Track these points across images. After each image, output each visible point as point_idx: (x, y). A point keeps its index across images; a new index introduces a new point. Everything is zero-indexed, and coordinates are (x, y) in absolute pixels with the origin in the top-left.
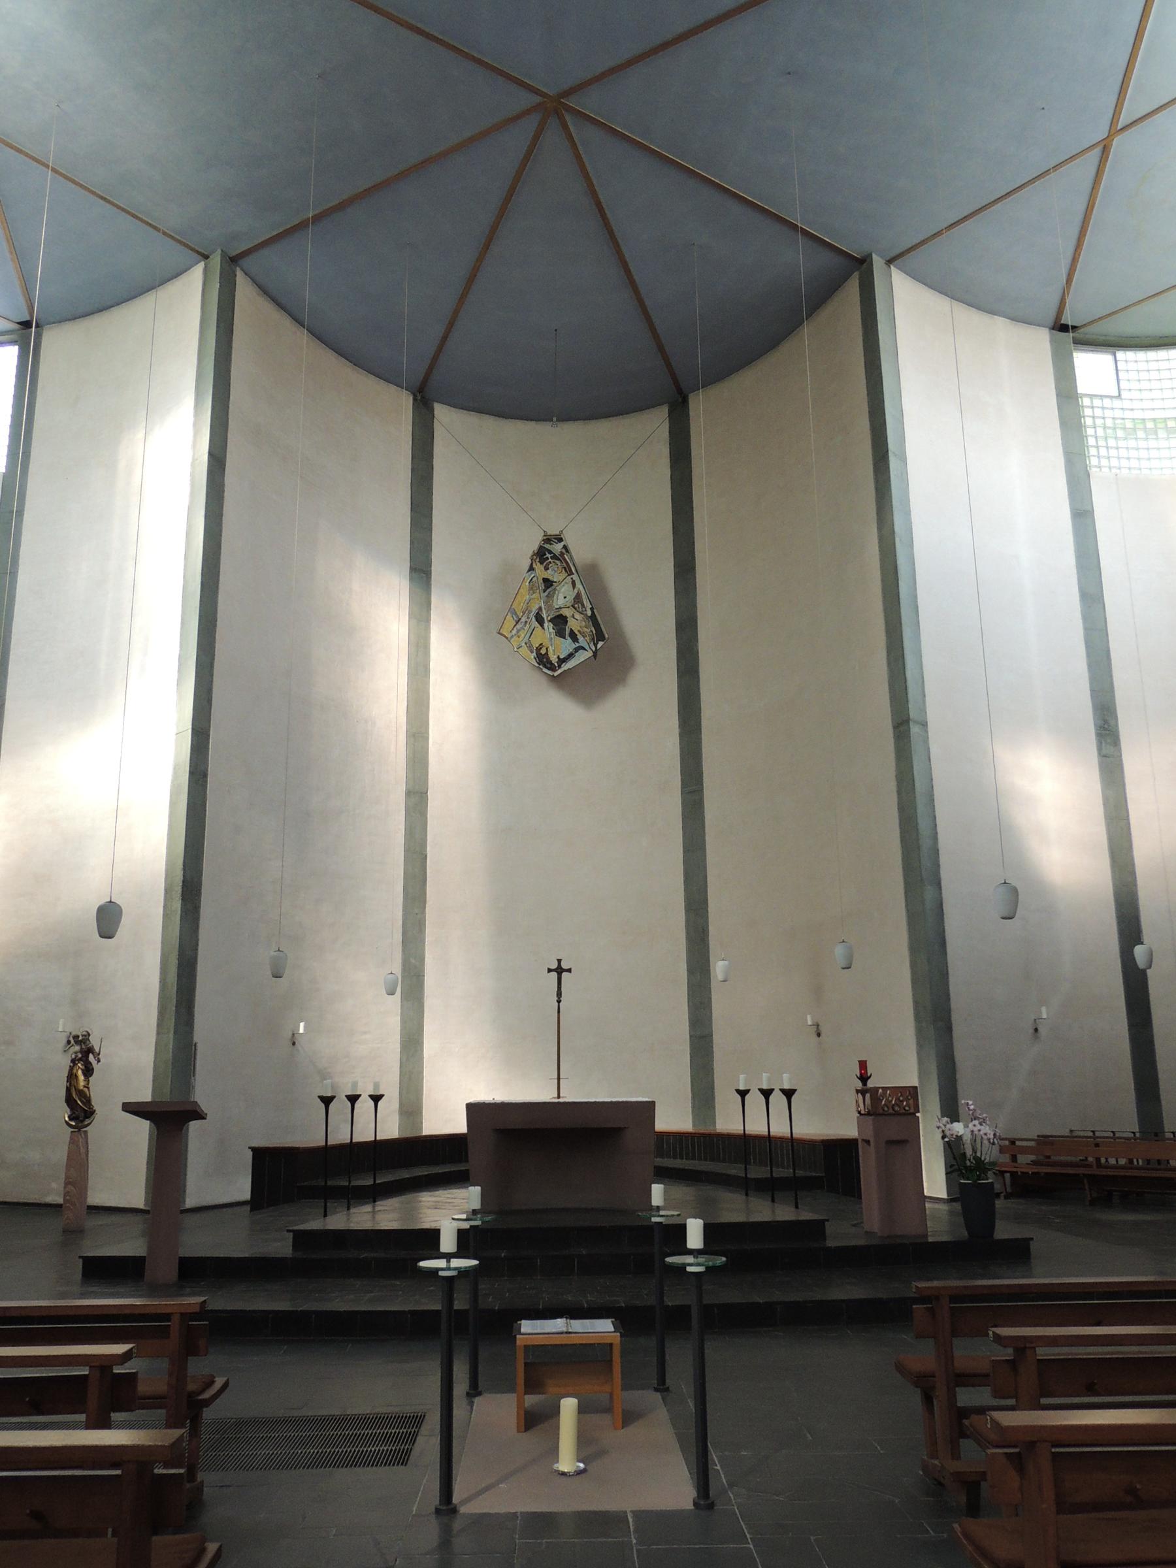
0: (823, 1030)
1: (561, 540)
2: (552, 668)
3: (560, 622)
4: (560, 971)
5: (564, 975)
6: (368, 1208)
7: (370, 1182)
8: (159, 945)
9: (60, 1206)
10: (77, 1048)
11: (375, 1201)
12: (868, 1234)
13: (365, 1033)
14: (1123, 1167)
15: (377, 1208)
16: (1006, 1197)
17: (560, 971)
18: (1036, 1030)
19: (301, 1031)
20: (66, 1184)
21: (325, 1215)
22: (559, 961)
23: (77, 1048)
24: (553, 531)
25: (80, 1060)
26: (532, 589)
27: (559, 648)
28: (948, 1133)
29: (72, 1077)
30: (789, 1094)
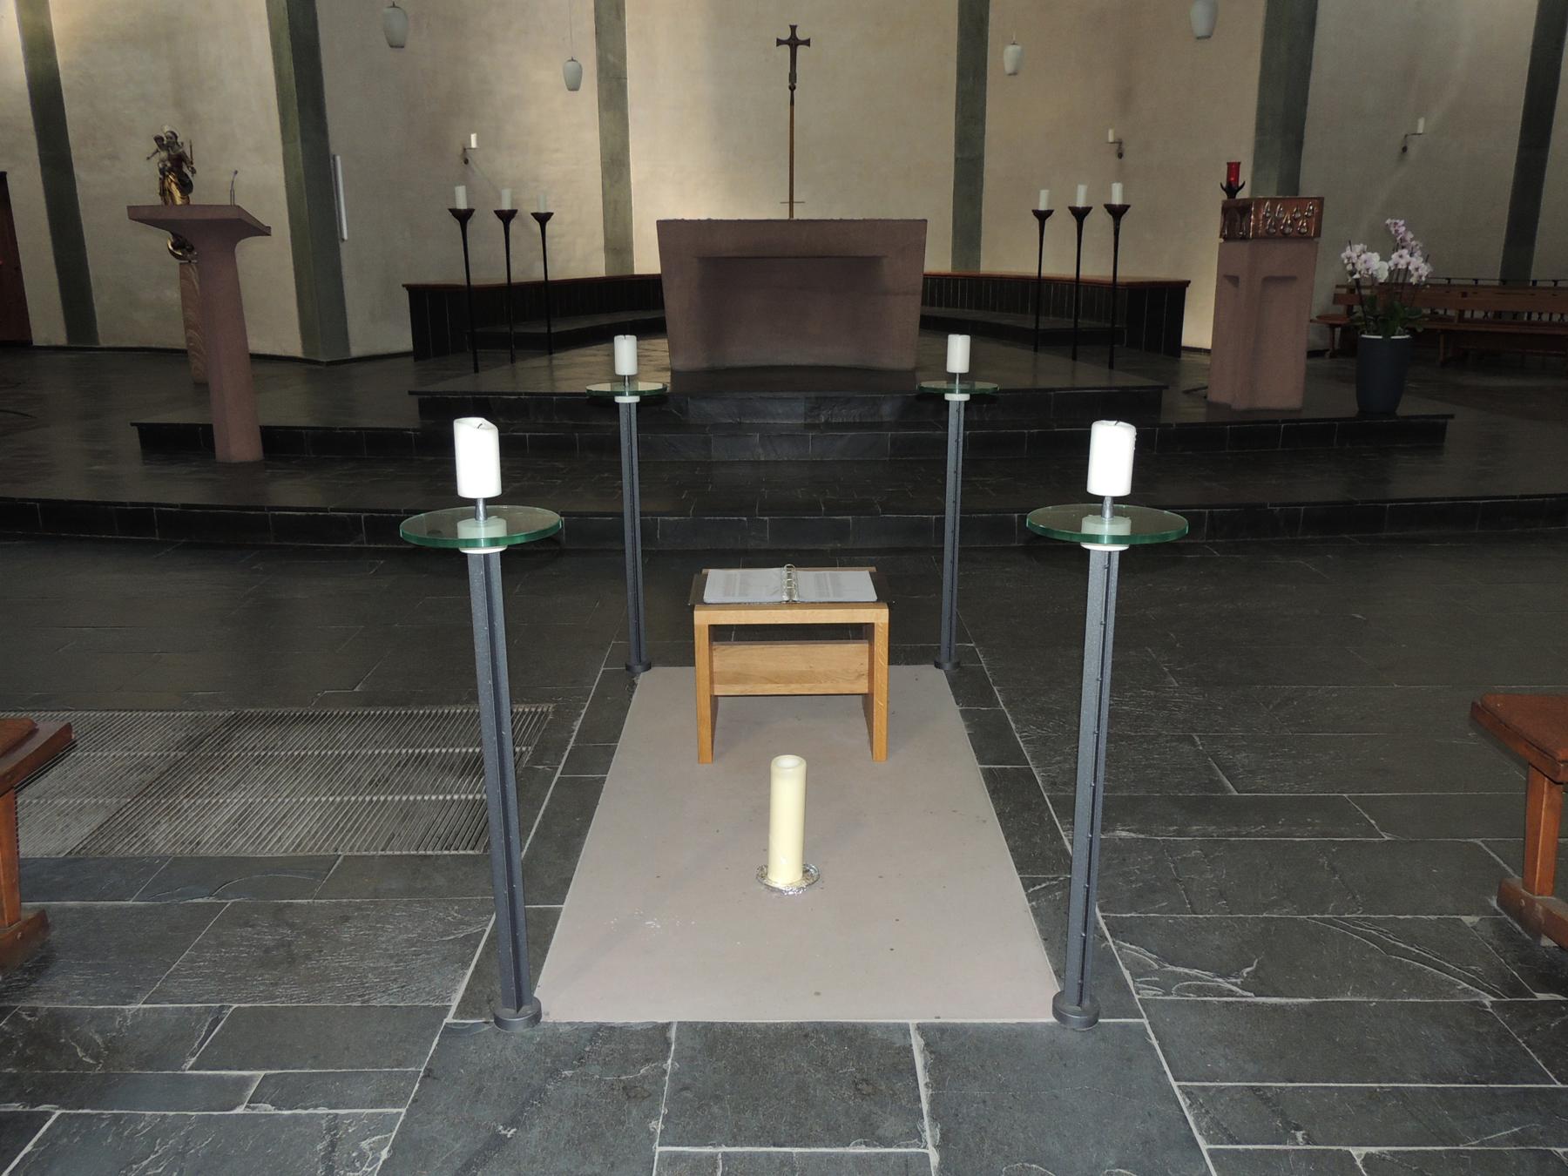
0: (1127, 149)
4: (793, 43)
5: (801, 50)
6: (542, 362)
7: (545, 330)
8: (266, 21)
9: (183, 352)
10: (164, 154)
11: (513, 361)
12: (1213, 406)
13: (557, 150)
14: (1478, 321)
15: (555, 362)
16: (1332, 356)
17: (793, 43)
18: (1405, 149)
19: (474, 145)
20: (187, 327)
21: (476, 371)
22: (793, 28)
23: (164, 154)
25: (170, 171)
28: (1359, 267)
30: (1117, 212)
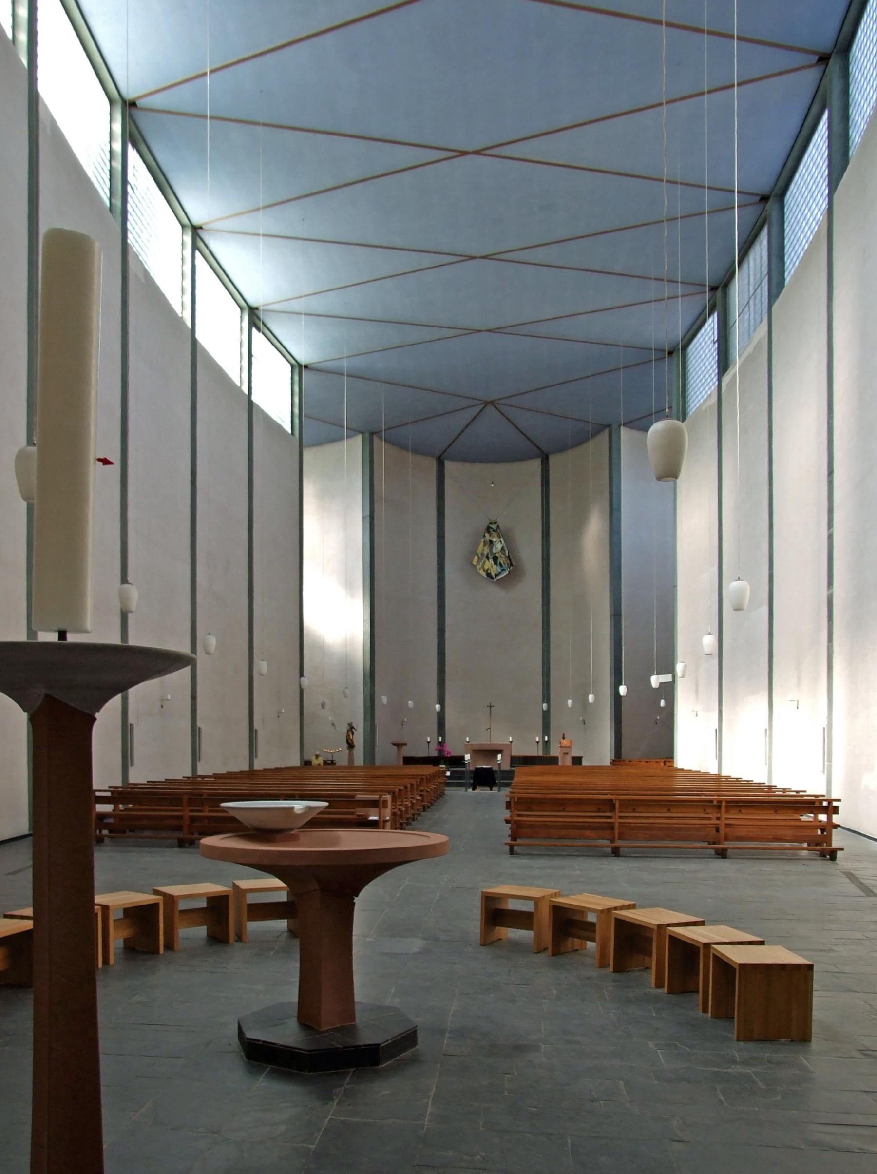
1: (496, 523)
2: (492, 578)
3: (495, 559)
4: (491, 706)
24: (493, 519)
26: (485, 545)
27: (495, 570)
29: (348, 736)
